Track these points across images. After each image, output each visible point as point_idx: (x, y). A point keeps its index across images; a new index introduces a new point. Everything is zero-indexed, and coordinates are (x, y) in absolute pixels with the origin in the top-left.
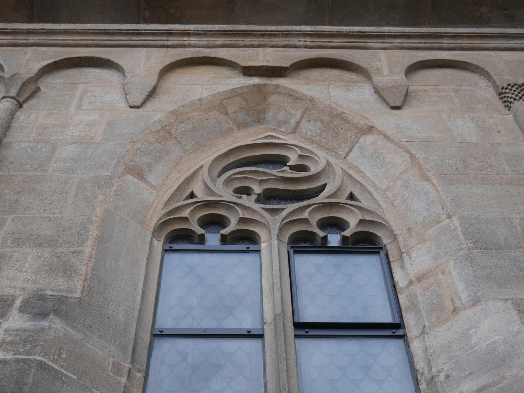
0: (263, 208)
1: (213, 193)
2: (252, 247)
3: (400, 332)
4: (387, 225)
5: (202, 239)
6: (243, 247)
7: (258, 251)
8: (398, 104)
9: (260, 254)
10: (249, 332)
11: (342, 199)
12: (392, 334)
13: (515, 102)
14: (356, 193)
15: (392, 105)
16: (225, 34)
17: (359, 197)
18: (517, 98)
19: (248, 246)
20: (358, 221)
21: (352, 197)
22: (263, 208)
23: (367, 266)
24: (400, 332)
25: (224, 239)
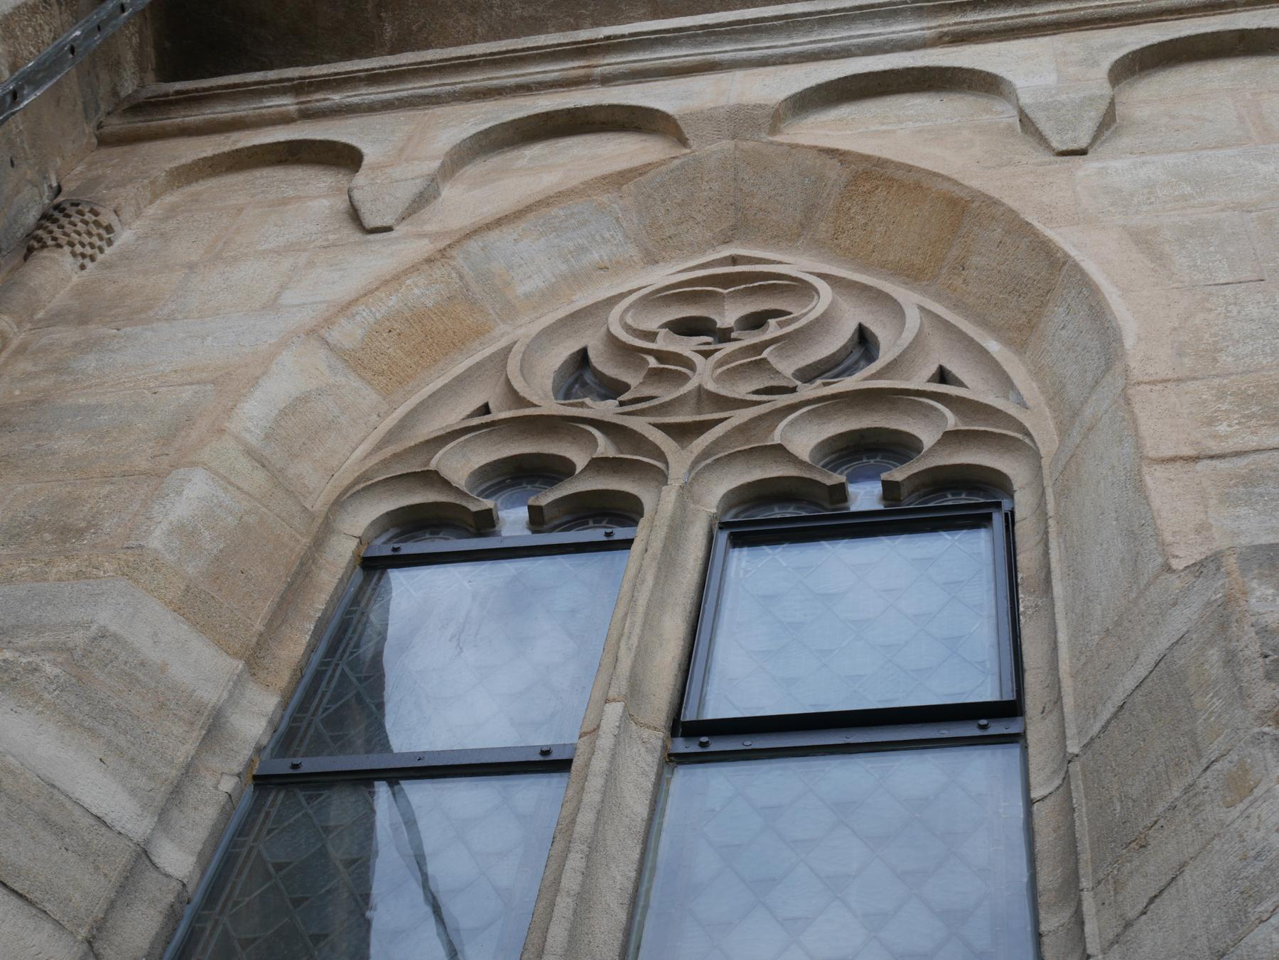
0: (655, 425)
1: (521, 402)
2: (620, 533)
3: (1012, 727)
4: (1031, 444)
5: (486, 523)
6: (595, 534)
7: (1017, 739)
8: (1083, 143)
9: (1025, 748)
10: (545, 753)
11: (919, 380)
12: (978, 732)
13: (67, 249)
14: (954, 368)
15: (1057, 144)
16: (728, 33)
17: (959, 376)
18: (78, 249)
19: (609, 531)
20: (939, 436)
21: (942, 376)
22: (655, 425)
23: (964, 555)
24: (1012, 727)
25: (537, 519)
